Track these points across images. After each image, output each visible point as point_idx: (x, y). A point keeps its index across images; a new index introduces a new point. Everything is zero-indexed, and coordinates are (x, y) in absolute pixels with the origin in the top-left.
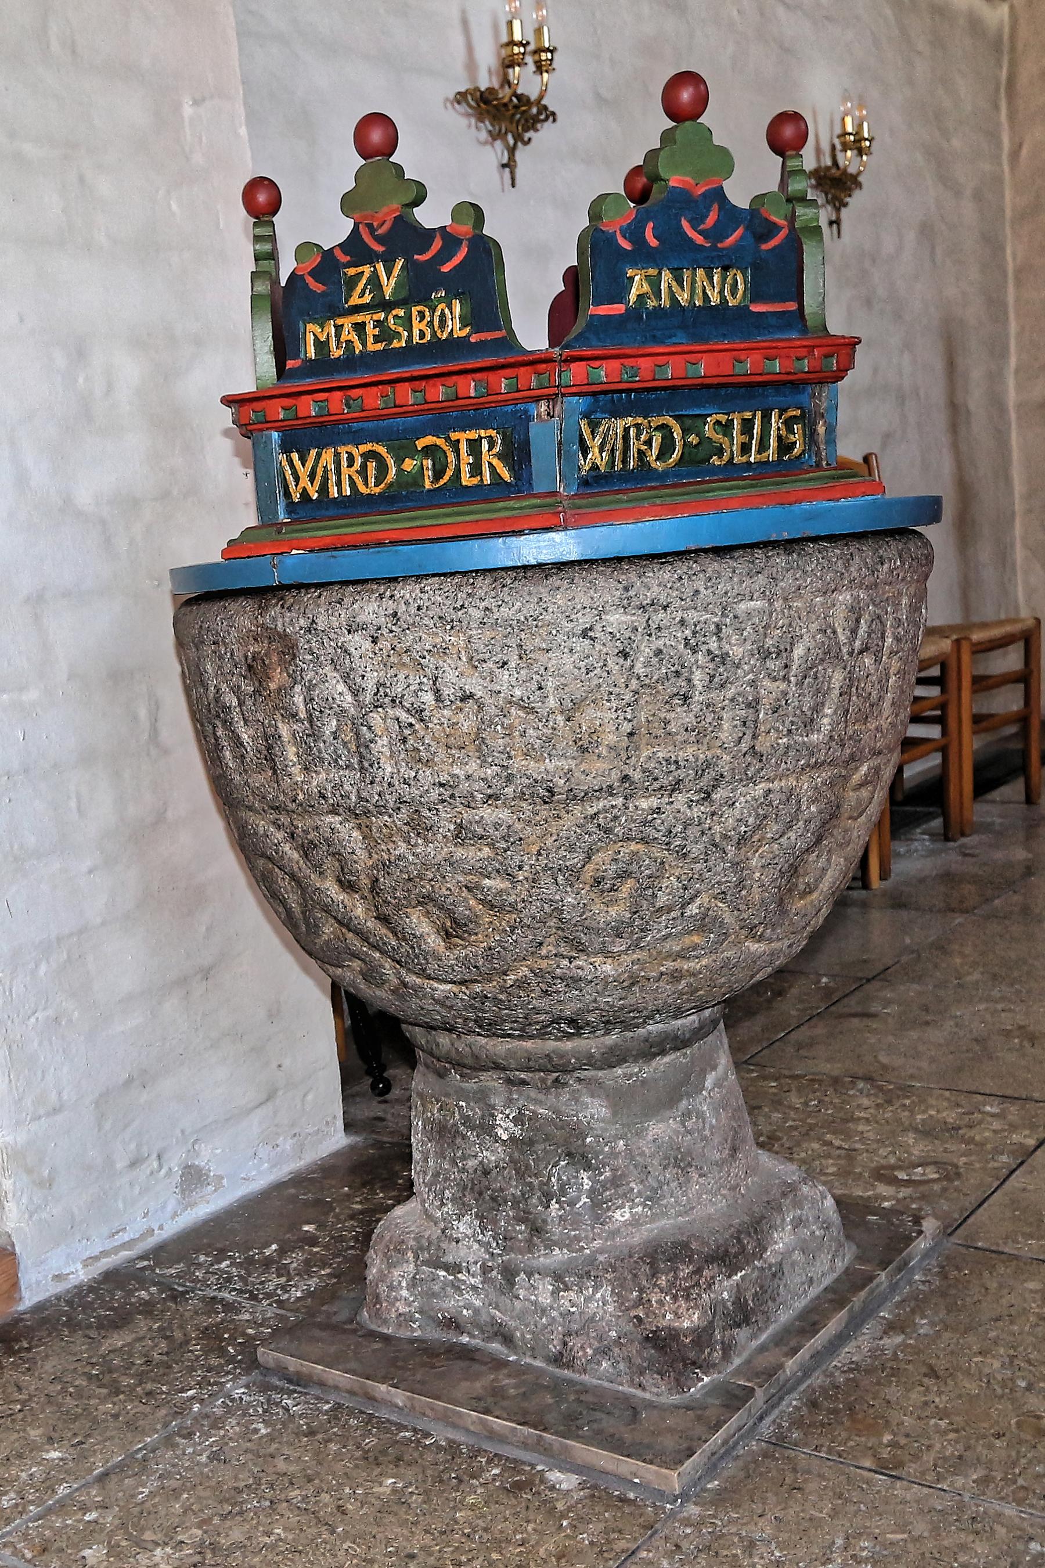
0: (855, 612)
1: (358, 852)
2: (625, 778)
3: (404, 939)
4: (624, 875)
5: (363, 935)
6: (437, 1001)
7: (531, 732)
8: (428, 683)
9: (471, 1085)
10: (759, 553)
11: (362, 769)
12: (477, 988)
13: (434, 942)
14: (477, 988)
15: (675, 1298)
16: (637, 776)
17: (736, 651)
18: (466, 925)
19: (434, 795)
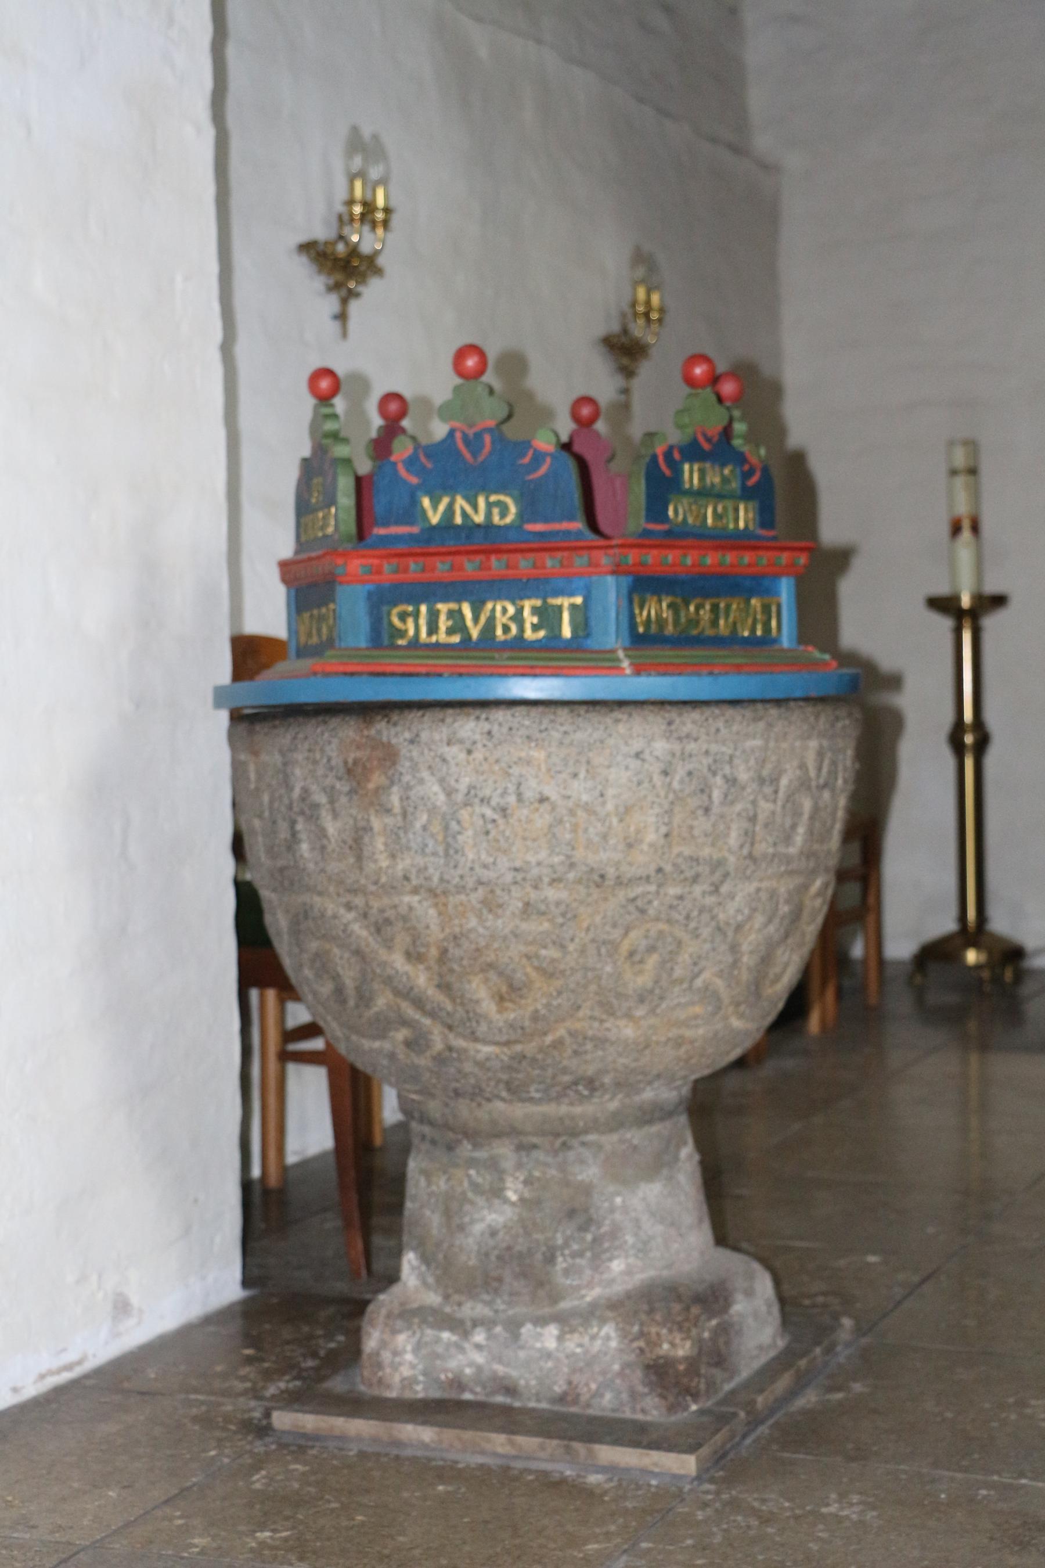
0: (820, 754)
1: (432, 927)
2: (660, 870)
3: (462, 1004)
4: (652, 949)
5: (419, 1003)
6: (477, 1063)
7: (591, 830)
8: (512, 788)
9: (481, 1154)
10: (759, 706)
11: (447, 854)
12: (518, 1048)
13: (488, 1006)
14: (518, 1048)
15: (670, 1331)
16: (668, 868)
17: (743, 776)
18: (520, 989)
19: (509, 877)
